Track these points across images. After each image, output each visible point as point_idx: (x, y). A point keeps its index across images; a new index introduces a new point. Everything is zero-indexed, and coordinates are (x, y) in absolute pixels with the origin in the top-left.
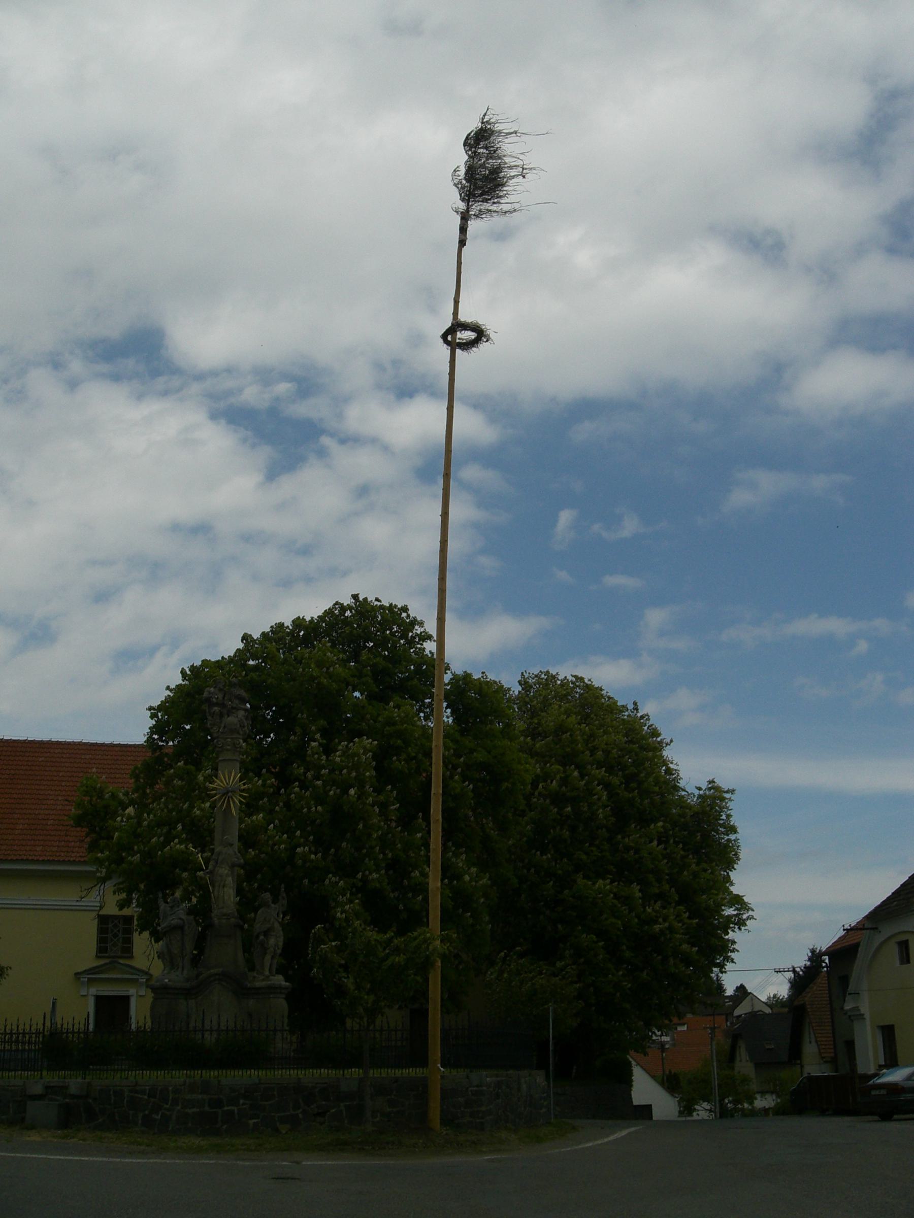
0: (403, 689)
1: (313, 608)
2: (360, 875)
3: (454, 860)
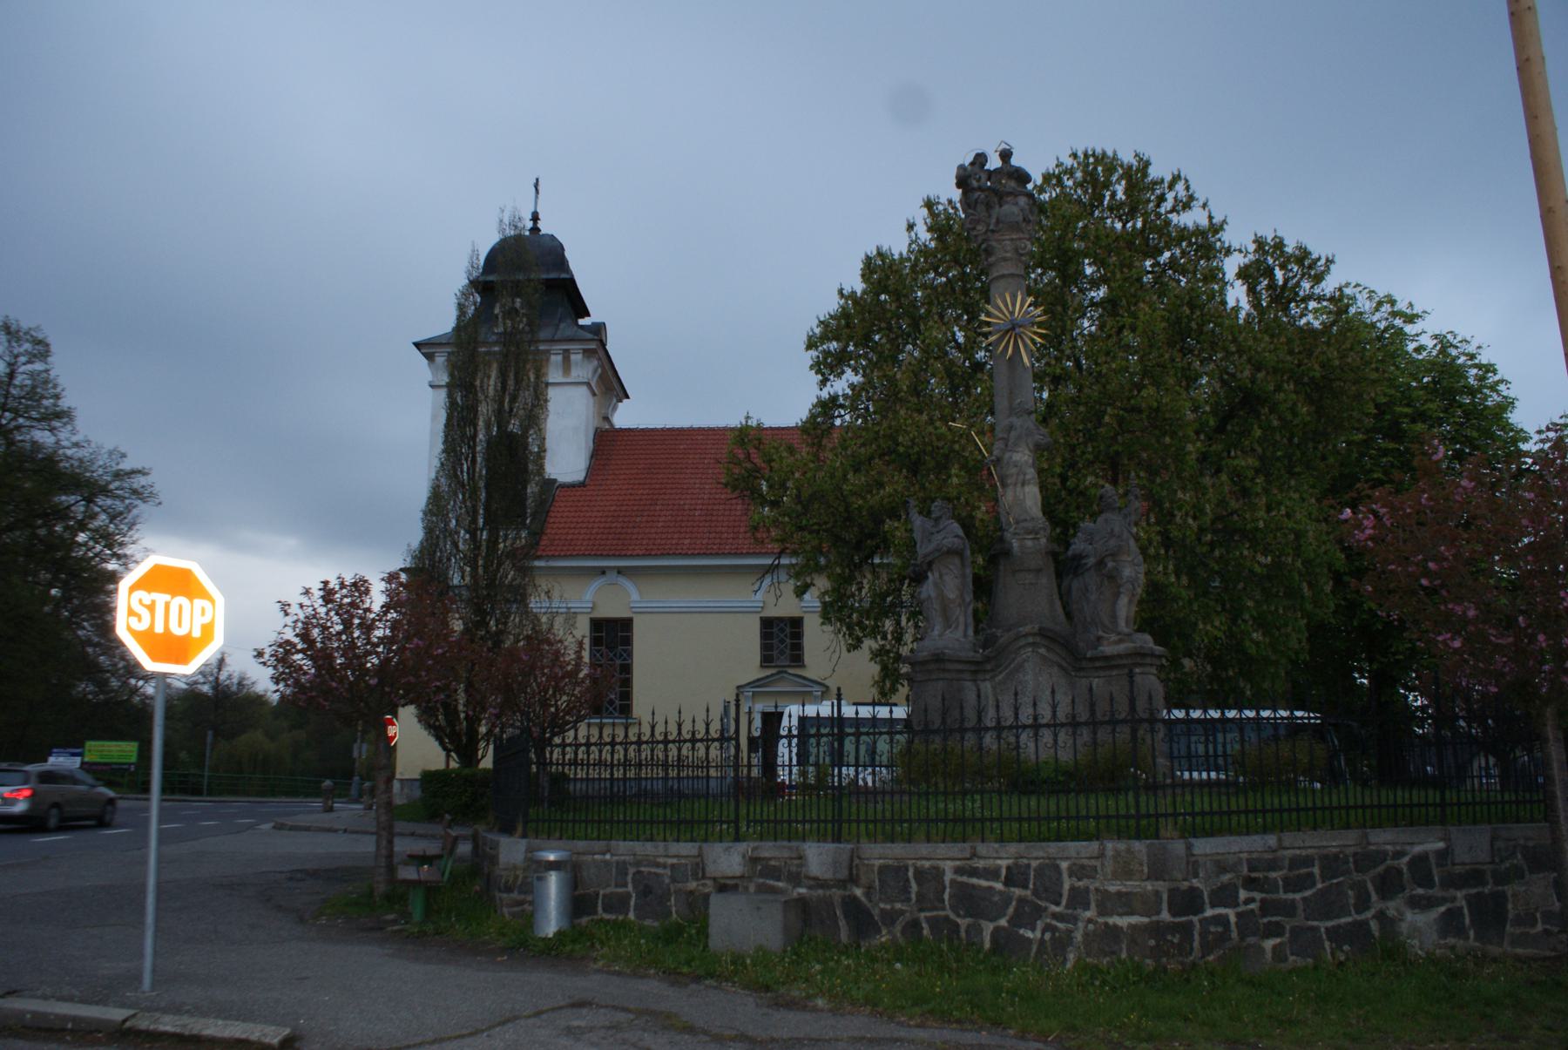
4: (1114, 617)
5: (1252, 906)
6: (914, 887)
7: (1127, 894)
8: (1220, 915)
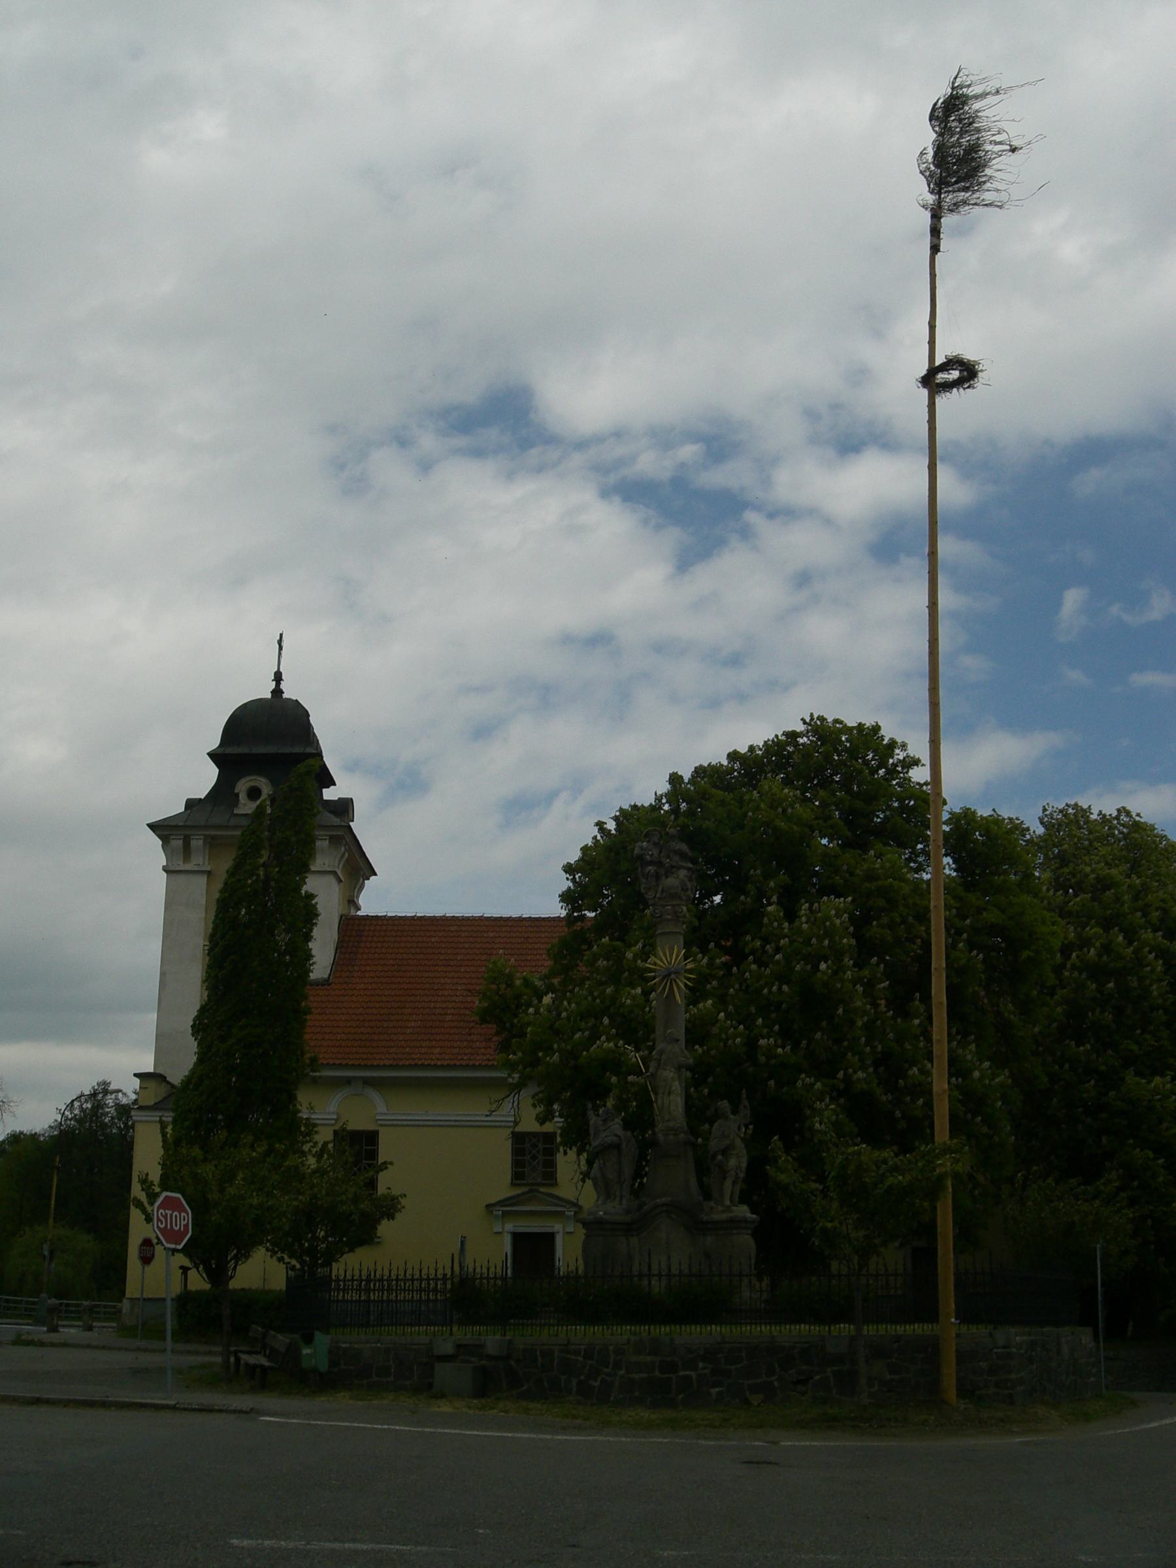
0: (886, 833)
1: (752, 731)
2: (841, 1074)
3: (960, 1051)
6: (540, 1359)
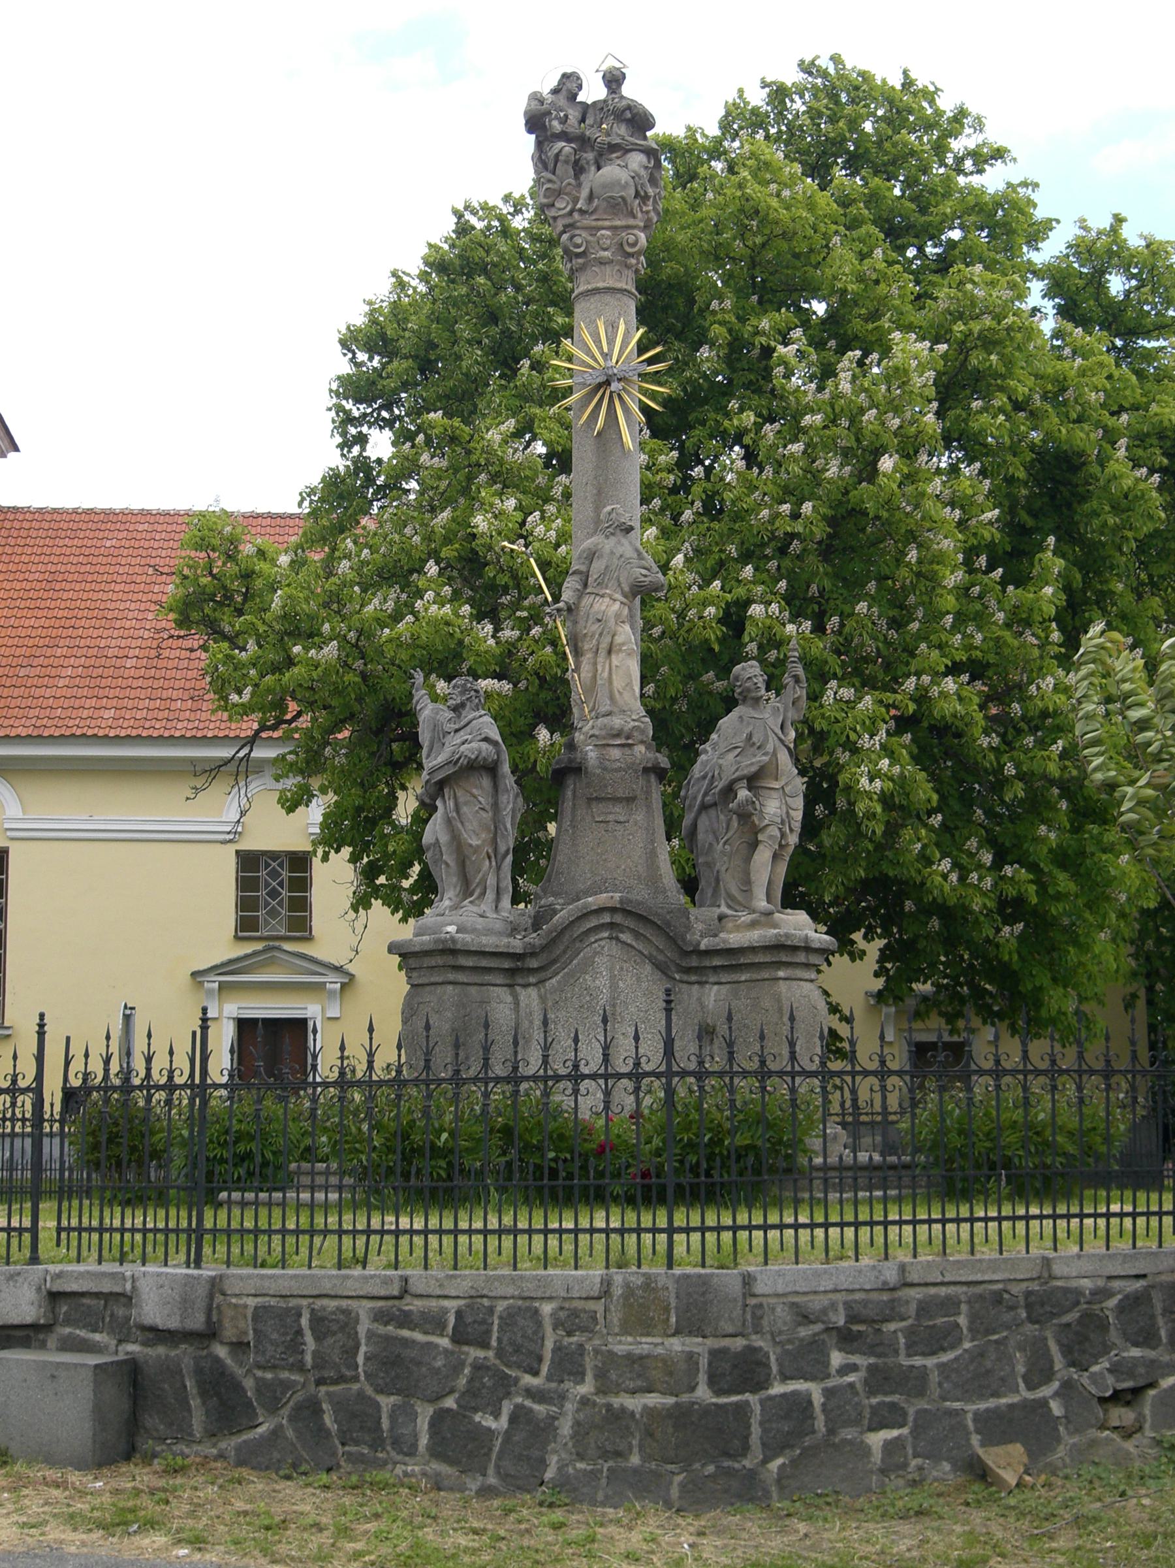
2: (910, 684)
4: (747, 883)
5: (851, 1378)
6: (309, 1338)
7: (642, 1357)
8: (794, 1393)
